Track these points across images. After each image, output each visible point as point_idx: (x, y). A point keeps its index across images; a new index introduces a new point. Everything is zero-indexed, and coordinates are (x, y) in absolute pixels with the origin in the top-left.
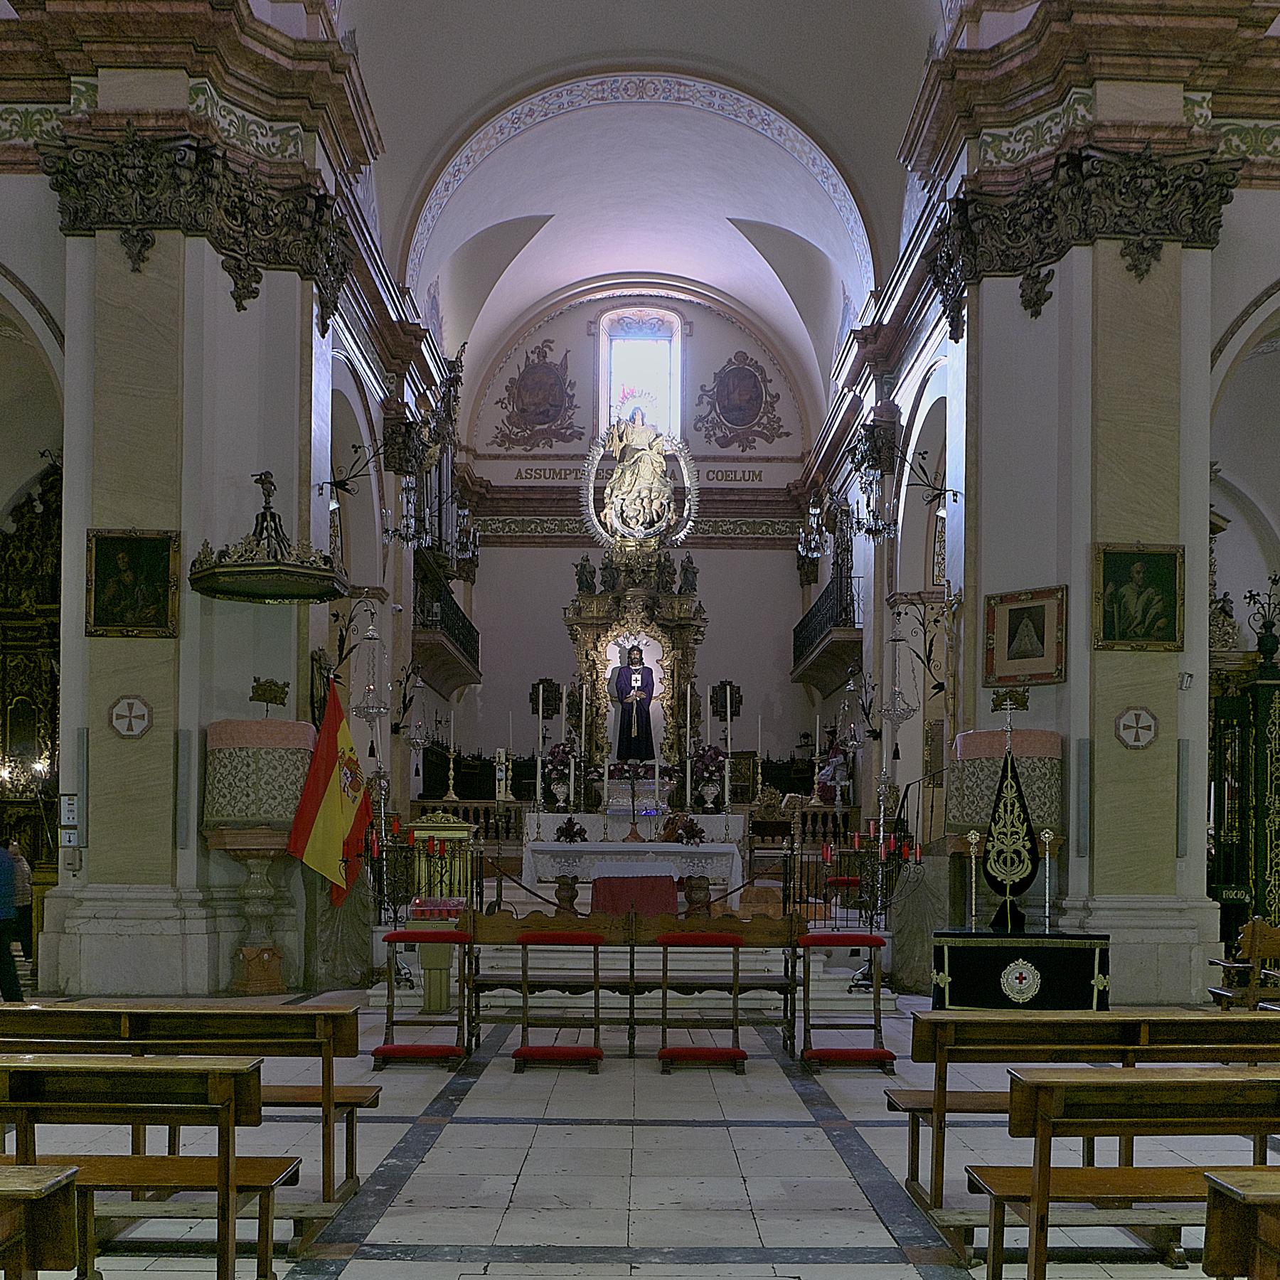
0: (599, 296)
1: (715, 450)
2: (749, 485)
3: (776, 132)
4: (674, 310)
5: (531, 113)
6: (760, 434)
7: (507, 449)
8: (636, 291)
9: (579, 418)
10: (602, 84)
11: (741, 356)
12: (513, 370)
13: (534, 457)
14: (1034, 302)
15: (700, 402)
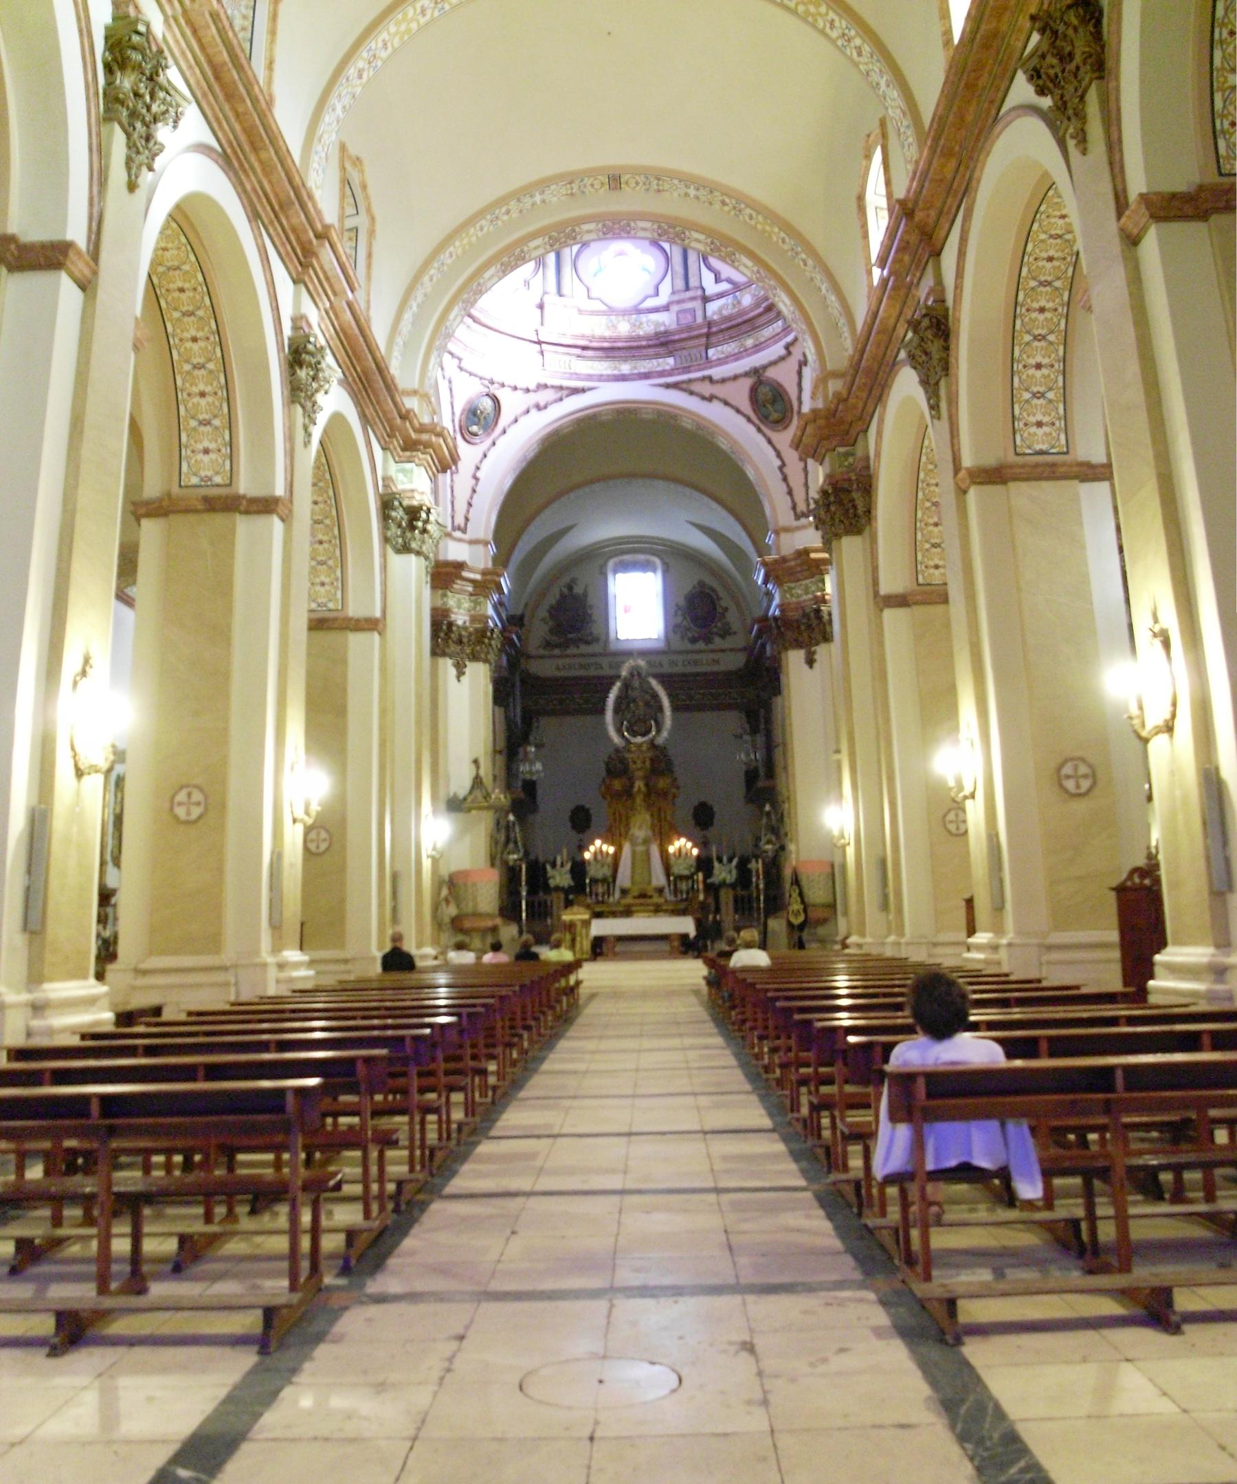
1: (690, 646)
4: (658, 556)
9: (596, 630)
11: (702, 584)
12: (552, 599)
14: (810, 662)
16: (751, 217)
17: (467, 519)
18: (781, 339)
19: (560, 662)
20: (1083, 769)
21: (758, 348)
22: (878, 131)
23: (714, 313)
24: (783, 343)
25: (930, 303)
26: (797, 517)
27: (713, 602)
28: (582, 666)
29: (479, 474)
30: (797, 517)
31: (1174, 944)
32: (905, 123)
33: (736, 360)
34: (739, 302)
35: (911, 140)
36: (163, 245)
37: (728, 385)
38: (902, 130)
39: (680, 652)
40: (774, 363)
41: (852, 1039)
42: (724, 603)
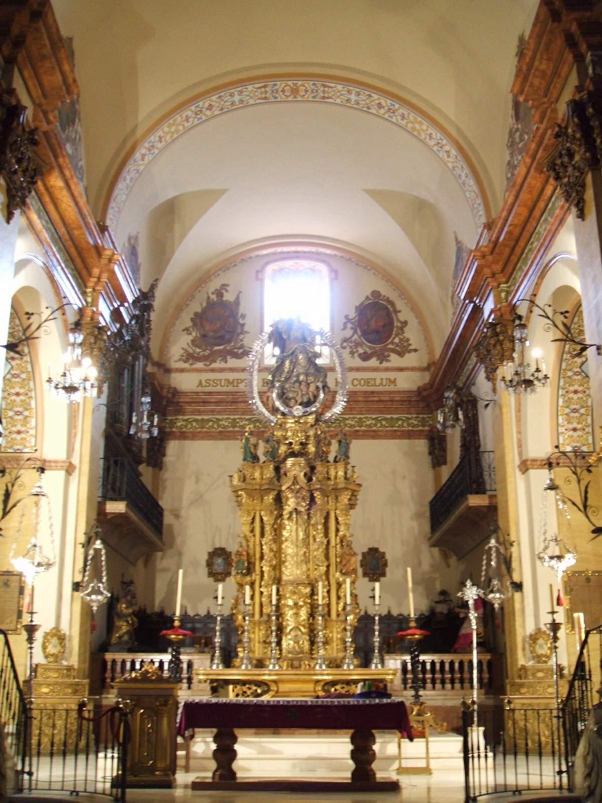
0: (265, 252)
2: (387, 388)
3: (399, 118)
4: (323, 261)
5: (210, 107)
6: (393, 351)
7: (191, 364)
8: (293, 249)
10: (265, 87)
11: (376, 294)
12: (196, 307)
13: (213, 370)
15: (345, 328)
19: (205, 376)
25: (490, 321)
27: (389, 314)
35: (481, 213)
42: (402, 317)
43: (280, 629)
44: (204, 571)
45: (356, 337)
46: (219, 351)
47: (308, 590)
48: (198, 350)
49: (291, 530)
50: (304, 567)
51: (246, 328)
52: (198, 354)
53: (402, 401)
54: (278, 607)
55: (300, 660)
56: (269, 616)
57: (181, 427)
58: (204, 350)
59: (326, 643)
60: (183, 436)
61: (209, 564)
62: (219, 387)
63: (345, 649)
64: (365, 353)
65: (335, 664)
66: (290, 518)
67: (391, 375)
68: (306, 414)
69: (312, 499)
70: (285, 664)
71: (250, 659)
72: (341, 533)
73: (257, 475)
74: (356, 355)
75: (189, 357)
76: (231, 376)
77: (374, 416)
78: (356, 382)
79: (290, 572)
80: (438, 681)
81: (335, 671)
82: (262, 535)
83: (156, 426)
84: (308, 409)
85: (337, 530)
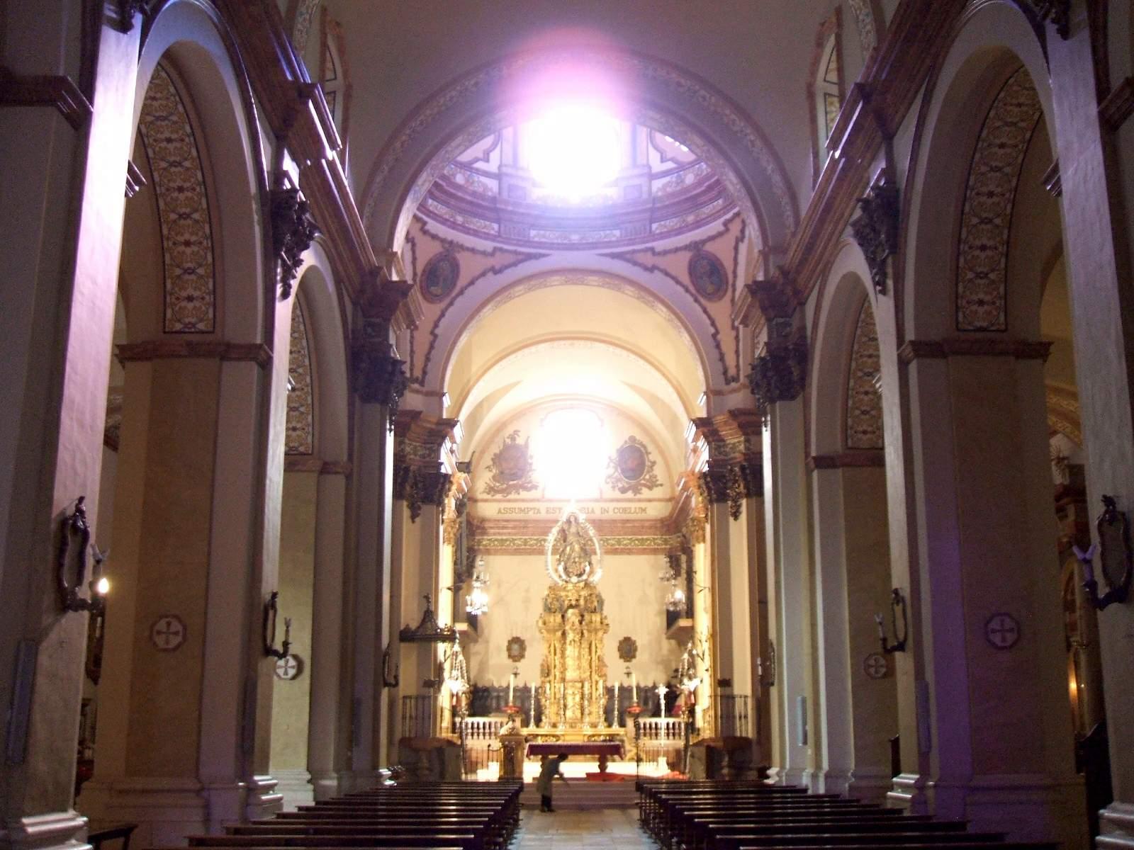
6: (645, 486)
11: (632, 439)
12: (495, 449)
13: (509, 501)
16: (704, 98)
17: (425, 373)
18: (720, 217)
19: (503, 505)
20: (1009, 623)
21: (698, 224)
22: (834, 20)
23: (659, 189)
24: (722, 219)
26: (728, 382)
28: (521, 510)
29: (437, 331)
30: (728, 382)
31: (1123, 801)
32: (865, 11)
33: (677, 235)
34: (682, 181)
35: (869, 27)
36: (152, 94)
37: (669, 257)
38: (861, 17)
39: (612, 500)
40: (712, 238)
41: (711, 826)
42: (651, 457)
43: (565, 706)
44: (505, 654)
45: (616, 474)
46: (514, 484)
47: (580, 685)
48: (498, 484)
49: (571, 651)
50: (578, 672)
51: (534, 467)
52: (498, 487)
53: (650, 527)
54: (564, 695)
55: (575, 723)
56: (559, 699)
57: (485, 546)
58: (502, 484)
59: (590, 714)
60: (488, 552)
61: (509, 649)
62: (514, 514)
63: (599, 717)
64: (623, 487)
65: (594, 726)
66: (570, 644)
67: (643, 505)
68: (579, 582)
69: (582, 633)
70: (568, 726)
71: (550, 723)
72: (598, 654)
73: (552, 620)
74: (617, 488)
75: (491, 490)
76: (523, 505)
77: (630, 537)
78: (616, 511)
79: (571, 674)
80: (671, 734)
81: (593, 729)
82: (555, 654)
83: (603, 767)
84: (580, 579)
85: (596, 652)
